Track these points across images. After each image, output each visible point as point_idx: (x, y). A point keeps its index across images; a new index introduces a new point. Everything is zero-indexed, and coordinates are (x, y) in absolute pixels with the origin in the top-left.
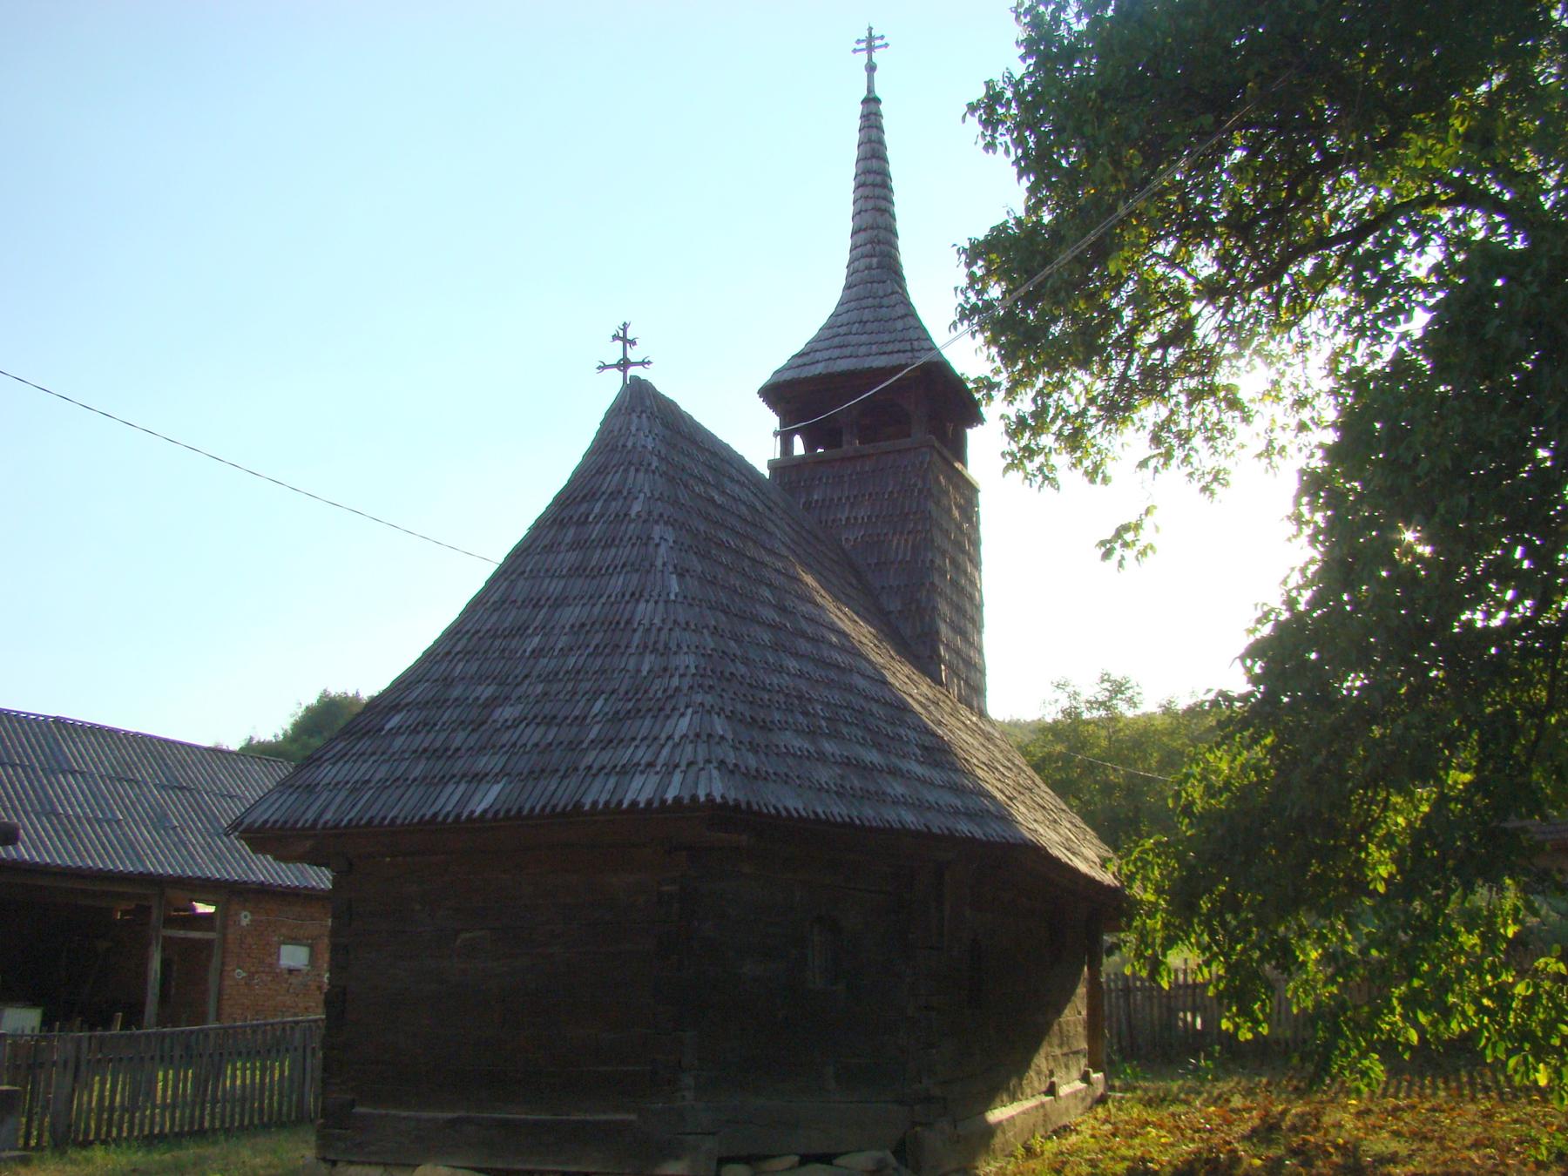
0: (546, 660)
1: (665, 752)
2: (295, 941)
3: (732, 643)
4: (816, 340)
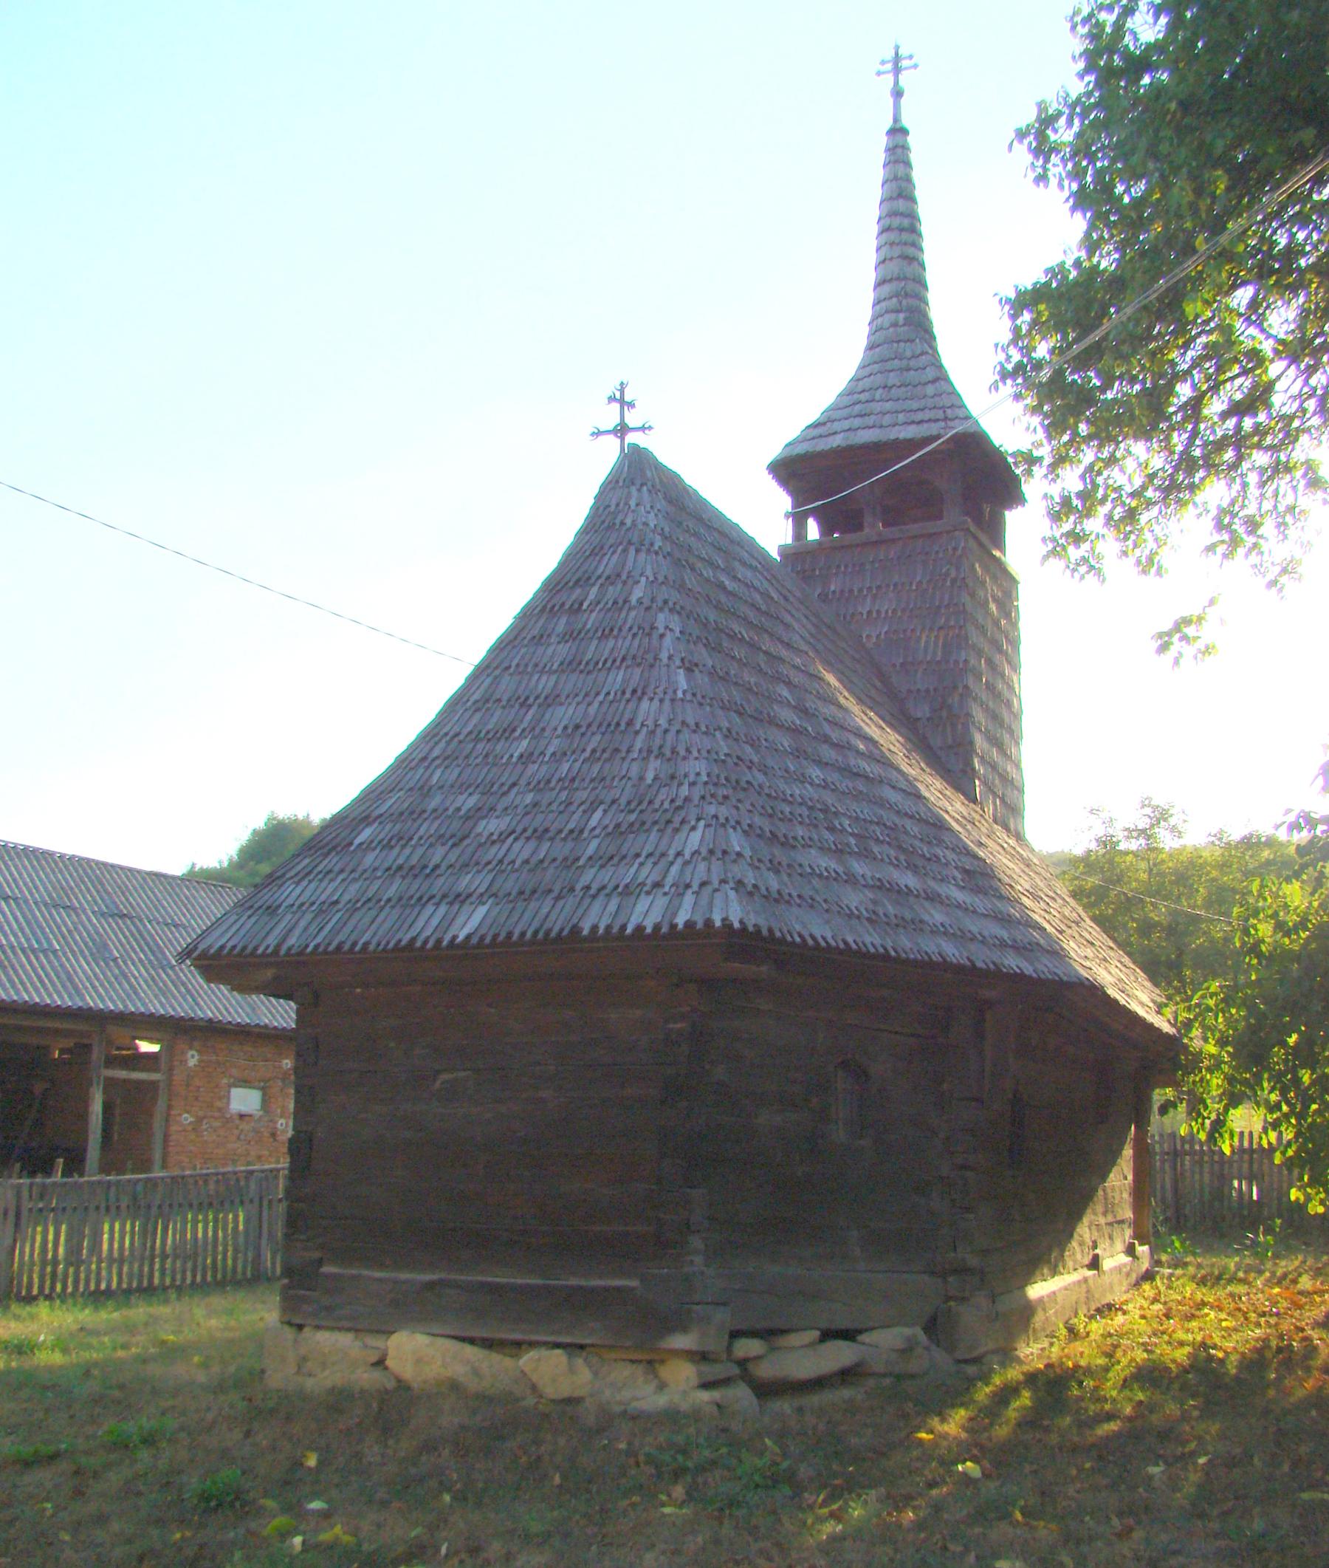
0: (536, 766)
1: (675, 870)
2: (246, 1083)
3: (748, 749)
4: (834, 408)
